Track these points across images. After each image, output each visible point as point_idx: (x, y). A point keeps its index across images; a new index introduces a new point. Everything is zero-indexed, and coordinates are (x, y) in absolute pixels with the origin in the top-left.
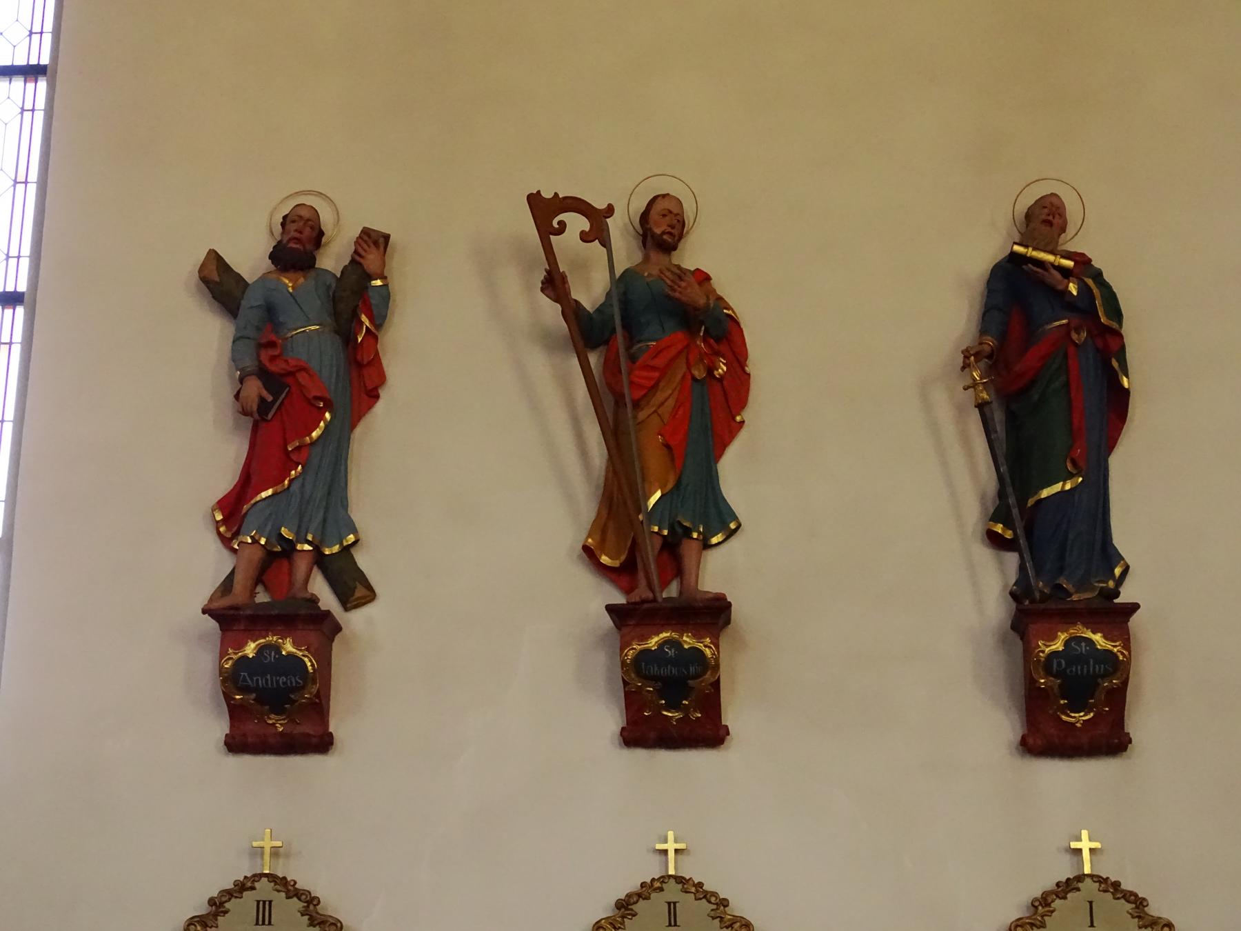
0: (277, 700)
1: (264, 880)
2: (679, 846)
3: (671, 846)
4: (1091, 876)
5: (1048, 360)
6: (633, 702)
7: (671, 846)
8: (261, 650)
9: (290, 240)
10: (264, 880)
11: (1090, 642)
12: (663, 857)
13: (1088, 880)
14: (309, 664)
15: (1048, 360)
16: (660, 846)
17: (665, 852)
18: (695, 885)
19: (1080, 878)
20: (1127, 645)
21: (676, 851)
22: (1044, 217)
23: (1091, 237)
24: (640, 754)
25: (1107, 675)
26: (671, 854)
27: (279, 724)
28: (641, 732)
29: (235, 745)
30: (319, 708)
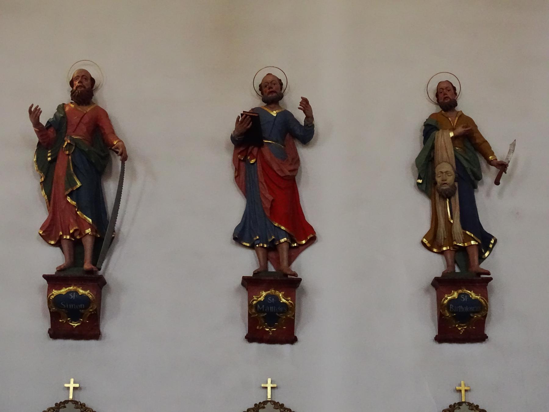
0: (271, 319)
1: (269, 403)
2: (466, 388)
3: (463, 388)
4: (71, 401)
5: (455, 162)
6: (54, 317)
7: (72, 385)
8: (460, 295)
9: (77, 88)
10: (70, 403)
11: (468, 295)
12: (67, 391)
13: (464, 404)
14: (482, 301)
15: (455, 162)
16: (458, 388)
17: (460, 391)
18: (475, 406)
19: (463, 402)
20: (485, 296)
21: (74, 388)
22: (268, 91)
23: (108, 99)
24: (60, 342)
25: (86, 308)
26: (463, 392)
27: (461, 329)
28: (446, 334)
29: (441, 338)
30: (481, 324)
